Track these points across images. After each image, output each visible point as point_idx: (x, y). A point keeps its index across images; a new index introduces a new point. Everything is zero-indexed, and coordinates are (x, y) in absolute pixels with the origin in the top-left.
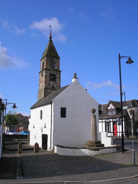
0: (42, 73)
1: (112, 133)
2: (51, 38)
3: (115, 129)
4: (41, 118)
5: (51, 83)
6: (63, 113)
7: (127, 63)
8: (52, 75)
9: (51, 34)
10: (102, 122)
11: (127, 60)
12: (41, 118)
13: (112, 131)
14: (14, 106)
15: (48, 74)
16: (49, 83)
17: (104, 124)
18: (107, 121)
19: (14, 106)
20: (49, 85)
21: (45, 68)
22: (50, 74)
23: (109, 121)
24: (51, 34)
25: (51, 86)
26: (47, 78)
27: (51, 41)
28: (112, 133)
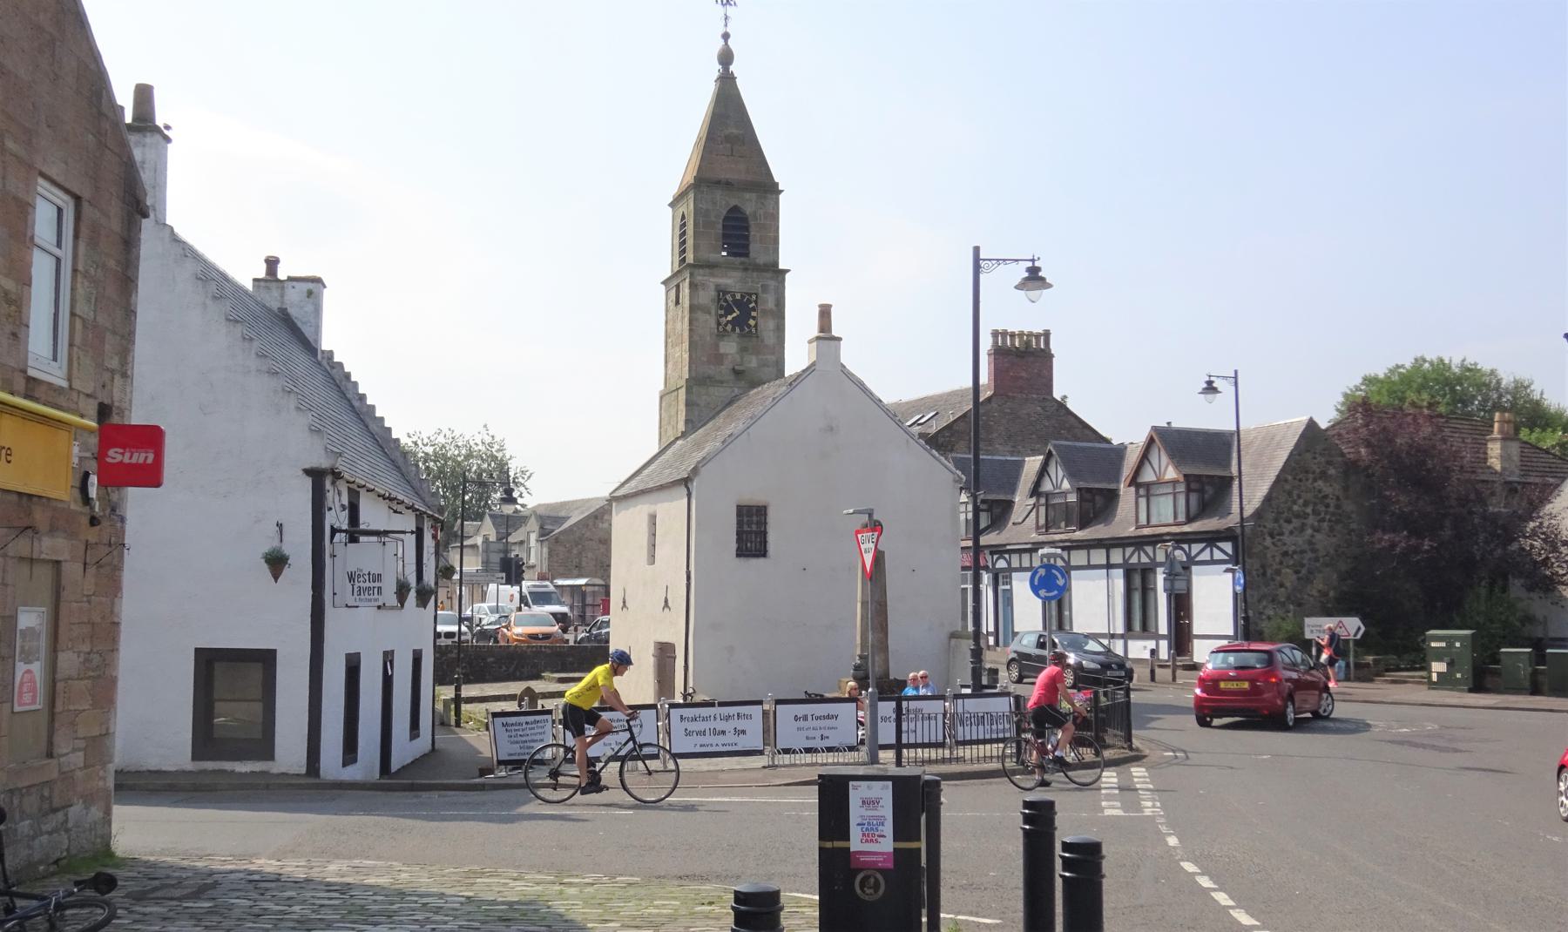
0: (678, 286)
1: (1163, 637)
2: (726, 58)
3: (1181, 605)
4: (652, 559)
5: (730, 347)
6: (752, 532)
7: (1021, 286)
8: (729, 297)
9: (726, 36)
10: (1109, 566)
11: (1021, 272)
12: (652, 559)
13: (1163, 629)
14: (1034, 278)
15: (707, 297)
16: (717, 346)
17: (1118, 575)
18: (1134, 560)
19: (1034, 278)
20: (719, 358)
21: (690, 258)
22: (721, 292)
23: (1145, 559)
24: (726, 36)
25: (725, 368)
26: (701, 316)
27: (727, 82)
28: (1163, 637)
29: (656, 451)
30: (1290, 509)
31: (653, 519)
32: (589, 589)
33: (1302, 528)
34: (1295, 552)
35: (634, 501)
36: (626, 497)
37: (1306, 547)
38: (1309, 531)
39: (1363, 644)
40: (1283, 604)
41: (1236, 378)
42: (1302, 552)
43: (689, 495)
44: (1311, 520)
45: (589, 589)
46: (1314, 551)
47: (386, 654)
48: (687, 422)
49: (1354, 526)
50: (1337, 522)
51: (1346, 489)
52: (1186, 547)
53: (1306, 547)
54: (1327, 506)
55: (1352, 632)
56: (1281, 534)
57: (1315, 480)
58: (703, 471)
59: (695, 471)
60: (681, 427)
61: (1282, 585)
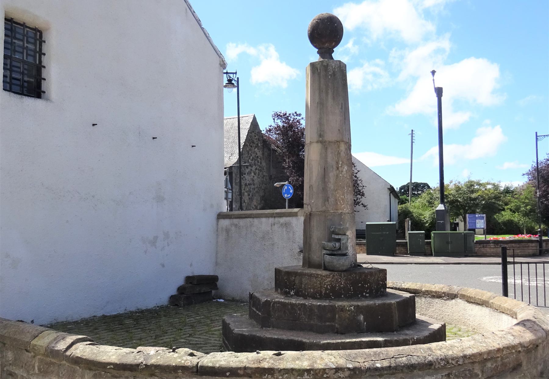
38: (253, 174)
42: (250, 184)
44: (254, 168)
49: (265, 174)
51: (263, 154)
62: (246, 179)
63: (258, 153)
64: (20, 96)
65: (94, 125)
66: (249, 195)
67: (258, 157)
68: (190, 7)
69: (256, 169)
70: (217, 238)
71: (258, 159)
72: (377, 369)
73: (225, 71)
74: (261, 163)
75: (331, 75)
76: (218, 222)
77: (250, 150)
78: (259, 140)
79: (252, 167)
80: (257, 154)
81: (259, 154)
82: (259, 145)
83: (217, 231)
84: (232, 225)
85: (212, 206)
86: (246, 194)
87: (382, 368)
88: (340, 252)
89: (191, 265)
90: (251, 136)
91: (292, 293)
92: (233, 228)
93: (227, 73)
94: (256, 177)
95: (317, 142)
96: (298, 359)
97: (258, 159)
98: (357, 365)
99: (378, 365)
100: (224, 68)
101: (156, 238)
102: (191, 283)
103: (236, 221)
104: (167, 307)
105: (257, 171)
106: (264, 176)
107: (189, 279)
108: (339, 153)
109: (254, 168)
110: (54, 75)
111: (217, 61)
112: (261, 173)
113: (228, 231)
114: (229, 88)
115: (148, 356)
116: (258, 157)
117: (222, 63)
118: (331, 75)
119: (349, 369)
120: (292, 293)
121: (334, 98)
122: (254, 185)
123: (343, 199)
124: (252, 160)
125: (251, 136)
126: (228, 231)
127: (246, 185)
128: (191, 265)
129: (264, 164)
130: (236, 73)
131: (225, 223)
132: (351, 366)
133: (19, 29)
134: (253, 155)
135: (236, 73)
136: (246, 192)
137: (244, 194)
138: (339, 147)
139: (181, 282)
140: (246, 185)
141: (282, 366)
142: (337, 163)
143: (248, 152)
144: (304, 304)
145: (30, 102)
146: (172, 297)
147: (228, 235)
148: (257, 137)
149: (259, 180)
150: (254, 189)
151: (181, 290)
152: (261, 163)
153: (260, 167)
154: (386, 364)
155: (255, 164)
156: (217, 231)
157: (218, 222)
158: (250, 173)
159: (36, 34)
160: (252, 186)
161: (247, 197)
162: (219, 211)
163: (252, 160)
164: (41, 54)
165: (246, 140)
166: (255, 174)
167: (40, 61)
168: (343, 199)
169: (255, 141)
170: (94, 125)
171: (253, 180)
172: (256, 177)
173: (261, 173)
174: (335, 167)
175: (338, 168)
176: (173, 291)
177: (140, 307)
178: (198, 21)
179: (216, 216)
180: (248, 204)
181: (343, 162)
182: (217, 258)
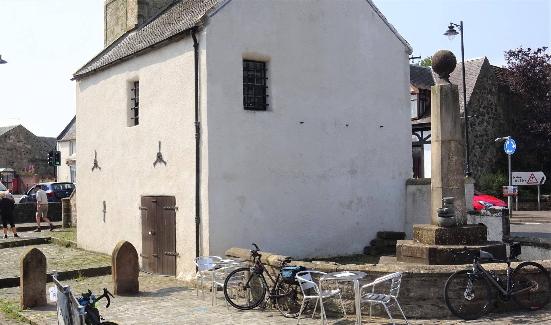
29: (103, 48)
30: (479, 110)
31: (135, 86)
32: (5, 174)
33: (482, 123)
34: (480, 136)
35: (106, 73)
36: (95, 72)
37: (483, 133)
38: (485, 124)
39: (545, 189)
40: (476, 166)
41: (462, 26)
42: (482, 136)
43: (196, 46)
44: (486, 118)
45: (5, 174)
46: (487, 135)
47: (137, 123)
48: (139, 16)
49: (501, 122)
50: (496, 119)
51: (499, 100)
52: (419, 133)
53: (483, 133)
54: (492, 109)
55: (539, 181)
56: (475, 125)
57: (488, 94)
58: (213, 20)
59: (205, 19)
60: (133, 21)
61: (475, 155)
62: (476, 131)
63: (491, 99)
64: (253, 112)
65: (301, 123)
66: (481, 148)
67: (491, 104)
68: (376, 10)
69: (490, 118)
70: (406, 201)
71: (492, 106)
72: (421, 274)
73: (410, 56)
74: (496, 110)
75: (444, 95)
76: (406, 187)
77: (481, 97)
78: (492, 84)
79: (484, 116)
80: (490, 101)
81: (494, 100)
82: (493, 90)
83: (406, 195)
84: (418, 190)
85: (401, 174)
86: (477, 146)
87: (424, 274)
88: (448, 215)
89: (382, 223)
90: (481, 82)
91: (418, 241)
92: (418, 193)
93: (412, 58)
94: (489, 127)
95: (436, 141)
96: (383, 267)
97: (492, 106)
98: (411, 271)
99: (422, 272)
100: (410, 53)
101: (351, 202)
102: (381, 237)
103: (419, 187)
104: (362, 255)
105: (491, 120)
106: (501, 124)
107: (380, 234)
108: (450, 148)
109: (486, 118)
110: (275, 91)
111: (403, 48)
112: (496, 122)
113: (414, 195)
114: (450, 35)
115: (316, 265)
116: (491, 104)
117: (407, 50)
118: (444, 95)
119: (406, 273)
120: (418, 241)
121: (446, 111)
122: (487, 135)
123: (453, 180)
124: (484, 108)
125: (481, 82)
126: (414, 195)
127: (476, 137)
128: (382, 223)
129: (500, 111)
130: (420, 57)
131: (412, 188)
132: (407, 272)
133: (251, 64)
134: (485, 103)
135: (420, 57)
136: (477, 144)
137: (473, 147)
138: (450, 144)
139: (373, 236)
140: (476, 137)
141: (374, 270)
142: (449, 155)
143: (478, 101)
144: (419, 247)
145: (260, 114)
146: (366, 248)
147: (414, 199)
148: (490, 82)
149: (494, 130)
150: (488, 140)
151: (373, 243)
152: (496, 110)
153: (494, 114)
154: (426, 272)
155: (488, 113)
156: (406, 195)
157: (406, 187)
158: (482, 123)
159: (261, 65)
160: (486, 138)
161: (479, 150)
162: (407, 178)
163: (484, 108)
164: (265, 78)
165: (475, 87)
166: (488, 123)
167: (265, 83)
168: (453, 180)
169: (487, 86)
170: (301, 123)
171: (486, 131)
172: (489, 127)
173: (496, 122)
174: (447, 158)
175: (449, 159)
176: (367, 243)
177: (340, 254)
178: (384, 20)
179: (405, 183)
180: (480, 158)
181: (453, 154)
182: (406, 216)
